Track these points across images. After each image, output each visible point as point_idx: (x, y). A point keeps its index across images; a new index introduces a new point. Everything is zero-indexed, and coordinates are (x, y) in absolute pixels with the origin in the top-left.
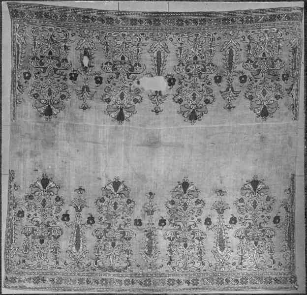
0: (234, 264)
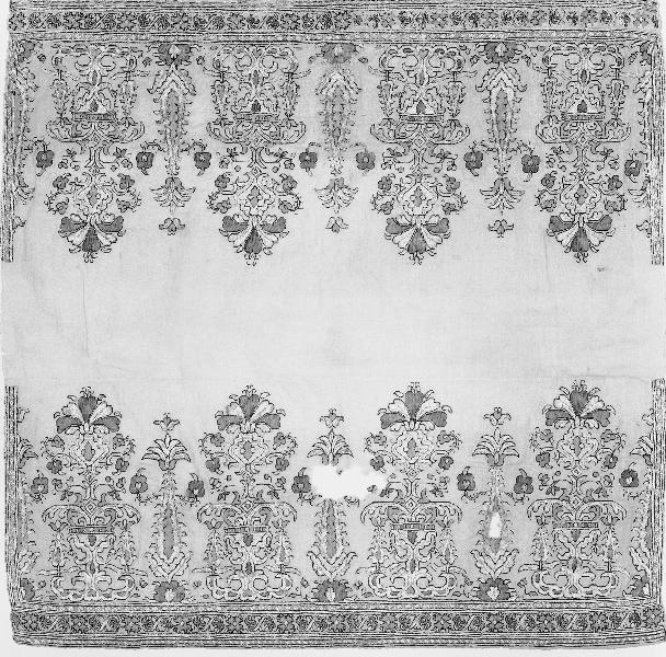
0: (147, 62)
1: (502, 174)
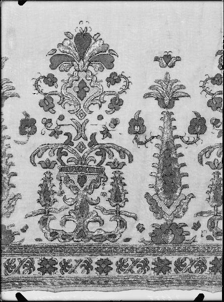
0: (197, 226)
1: (169, 118)
